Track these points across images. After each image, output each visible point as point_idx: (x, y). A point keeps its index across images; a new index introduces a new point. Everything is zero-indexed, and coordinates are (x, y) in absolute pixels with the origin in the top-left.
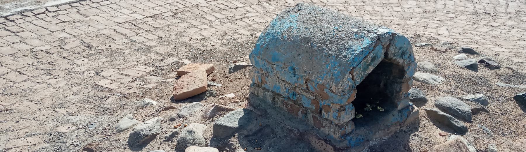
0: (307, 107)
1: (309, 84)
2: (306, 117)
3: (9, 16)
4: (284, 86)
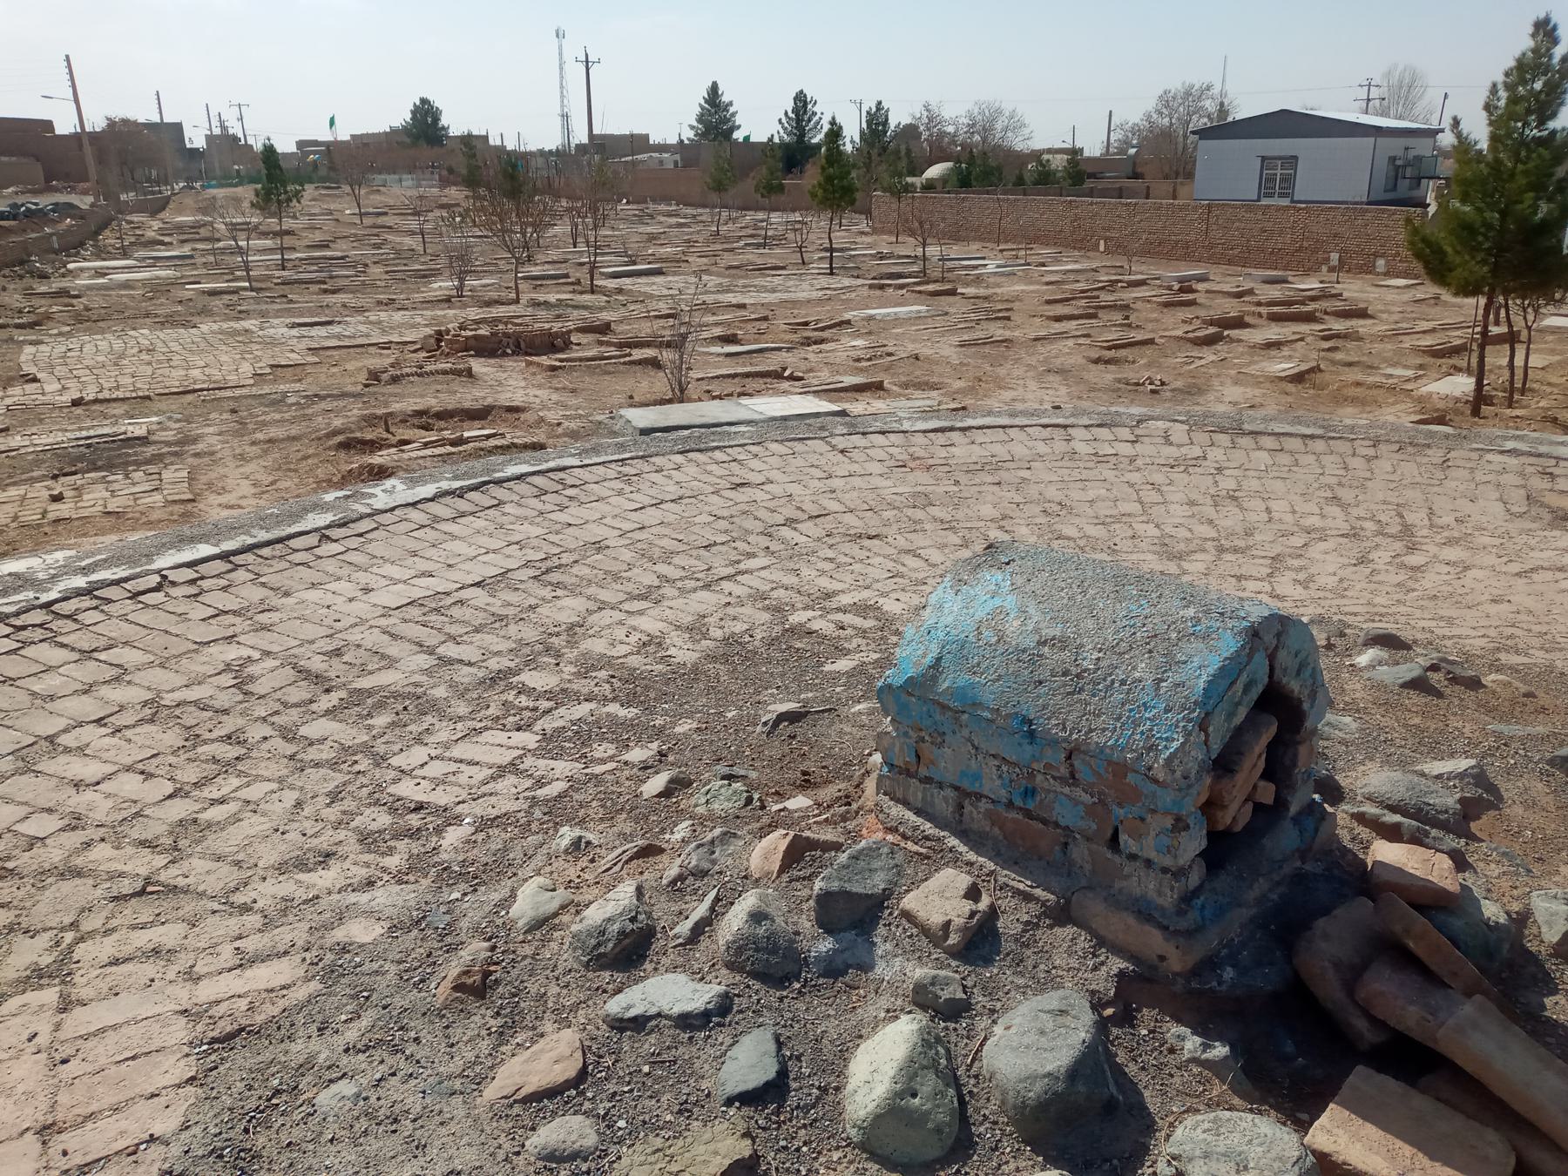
0: (1070, 825)
1: (1077, 763)
2: (1065, 853)
3: (56, 601)
4: (994, 769)
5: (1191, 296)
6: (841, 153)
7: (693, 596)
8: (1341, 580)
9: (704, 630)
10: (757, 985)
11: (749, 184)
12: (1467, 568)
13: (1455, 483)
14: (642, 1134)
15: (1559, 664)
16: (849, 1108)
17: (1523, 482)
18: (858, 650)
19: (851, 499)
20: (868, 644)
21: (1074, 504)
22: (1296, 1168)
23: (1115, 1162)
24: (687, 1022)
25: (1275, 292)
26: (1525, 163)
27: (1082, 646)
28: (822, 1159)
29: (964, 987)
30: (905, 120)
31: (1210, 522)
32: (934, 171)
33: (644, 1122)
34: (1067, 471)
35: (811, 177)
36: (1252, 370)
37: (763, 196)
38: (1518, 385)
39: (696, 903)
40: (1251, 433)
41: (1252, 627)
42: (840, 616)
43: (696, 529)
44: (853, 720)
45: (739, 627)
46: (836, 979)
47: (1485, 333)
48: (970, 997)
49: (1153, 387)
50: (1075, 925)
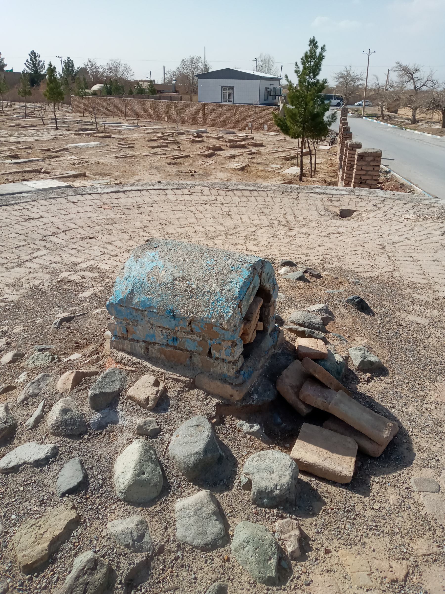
1: (193, 326)
2: (191, 361)
5: (201, 139)
6: (55, 78)
7: (13, 270)
8: (269, 243)
9: (20, 285)
10: (68, 440)
11: (15, 91)
12: (309, 235)
13: (302, 205)
14: (24, 519)
15: (343, 266)
16: (117, 485)
17: (323, 203)
18: (92, 286)
19: (80, 222)
20: (96, 284)
21: (171, 220)
22: (290, 468)
23: (225, 480)
24: (38, 464)
25: (230, 137)
26: (310, 91)
27: (190, 279)
28: (108, 510)
29: (157, 423)
30: (82, 66)
31: (222, 224)
32: (96, 87)
33: (25, 514)
34: (167, 207)
35: (43, 88)
36: (226, 166)
37: (22, 96)
38: (313, 170)
39: (34, 409)
40: (232, 190)
41: (253, 266)
42: (82, 273)
43: (10, 240)
44: (95, 317)
45: (37, 282)
46: (103, 430)
47: (302, 152)
48: (160, 427)
49: (192, 174)
50: (197, 388)
